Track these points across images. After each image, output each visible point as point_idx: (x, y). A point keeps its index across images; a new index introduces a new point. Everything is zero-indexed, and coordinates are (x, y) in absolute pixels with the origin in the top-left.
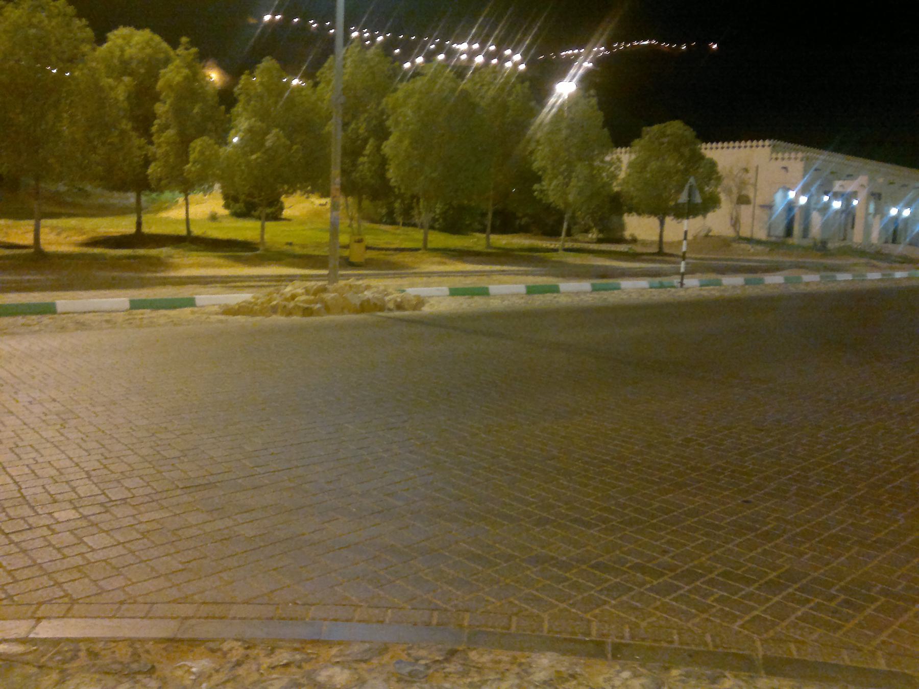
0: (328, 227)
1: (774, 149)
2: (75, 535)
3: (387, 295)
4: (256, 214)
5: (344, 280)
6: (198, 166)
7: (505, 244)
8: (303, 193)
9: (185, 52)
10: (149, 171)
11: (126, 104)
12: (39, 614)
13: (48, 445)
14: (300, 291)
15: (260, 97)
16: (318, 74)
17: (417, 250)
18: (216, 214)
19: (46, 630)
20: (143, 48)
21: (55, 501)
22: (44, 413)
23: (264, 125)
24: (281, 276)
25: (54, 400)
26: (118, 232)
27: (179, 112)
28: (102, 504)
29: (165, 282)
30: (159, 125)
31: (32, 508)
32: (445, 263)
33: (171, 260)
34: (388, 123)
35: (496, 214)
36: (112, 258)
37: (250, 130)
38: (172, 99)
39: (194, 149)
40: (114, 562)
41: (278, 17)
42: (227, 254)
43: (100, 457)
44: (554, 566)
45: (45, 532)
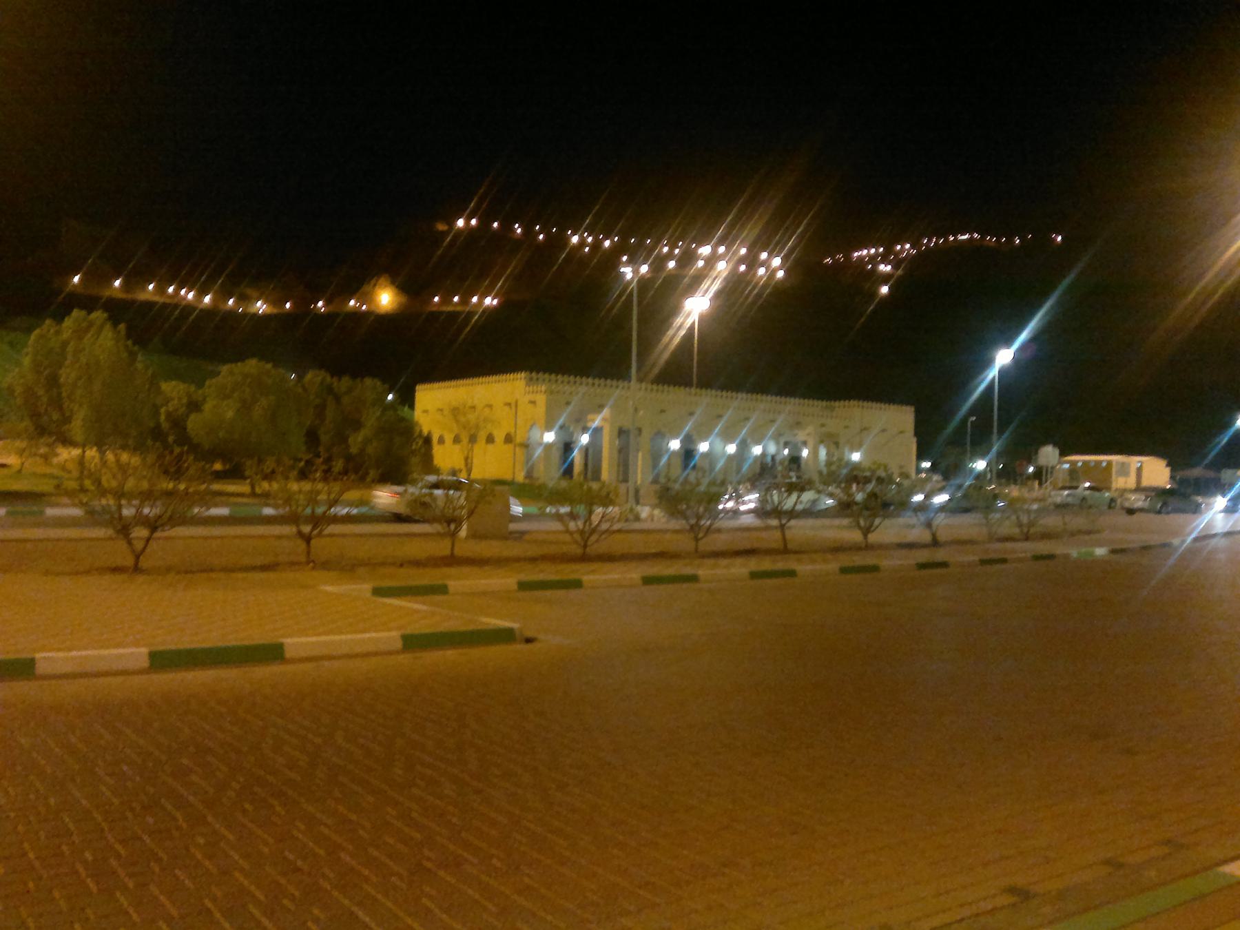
1: (530, 381)
41: (474, 222)
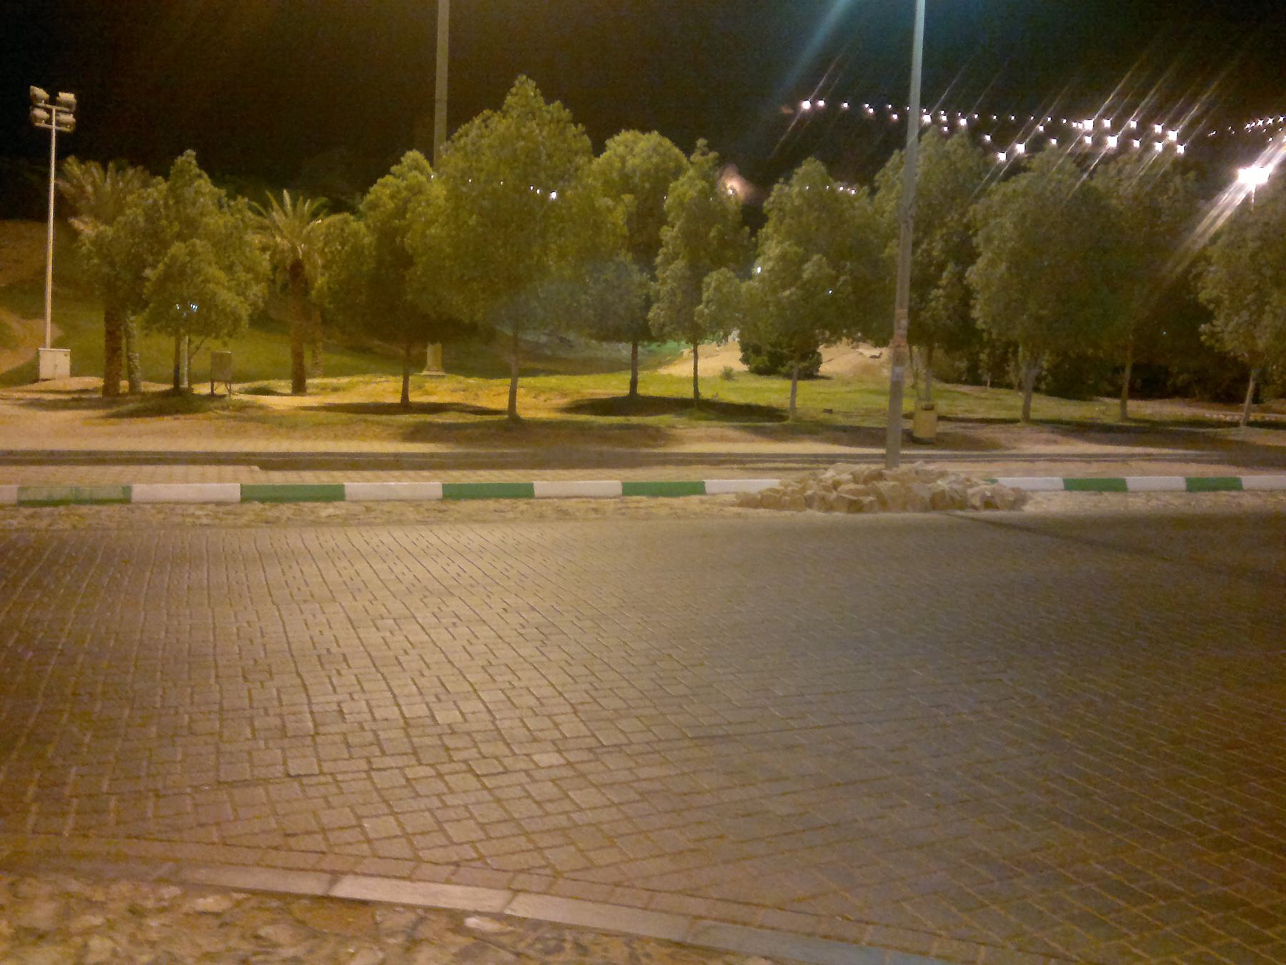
0: (888, 386)
2: (559, 787)
3: (971, 486)
4: (783, 370)
5: (905, 463)
6: (714, 308)
7: (1150, 415)
8: (850, 340)
9: (702, 157)
10: (651, 315)
11: (626, 231)
12: (516, 885)
13: (526, 665)
14: (846, 477)
15: (798, 212)
16: (877, 177)
17: (1014, 421)
18: (731, 370)
19: (524, 907)
20: (650, 157)
21: (535, 740)
22: (521, 624)
23: (801, 250)
24: (816, 456)
25: (533, 609)
26: (608, 395)
27: (692, 238)
28: (590, 750)
29: (665, 460)
30: (665, 254)
31: (508, 745)
32: (1056, 442)
33: (674, 431)
34: (975, 241)
35: (1135, 368)
36: (601, 427)
37: (783, 257)
38: (682, 220)
39: (709, 284)
40: (605, 827)
42: (747, 424)
43: (588, 687)
44: (1245, 916)
45: (523, 778)
